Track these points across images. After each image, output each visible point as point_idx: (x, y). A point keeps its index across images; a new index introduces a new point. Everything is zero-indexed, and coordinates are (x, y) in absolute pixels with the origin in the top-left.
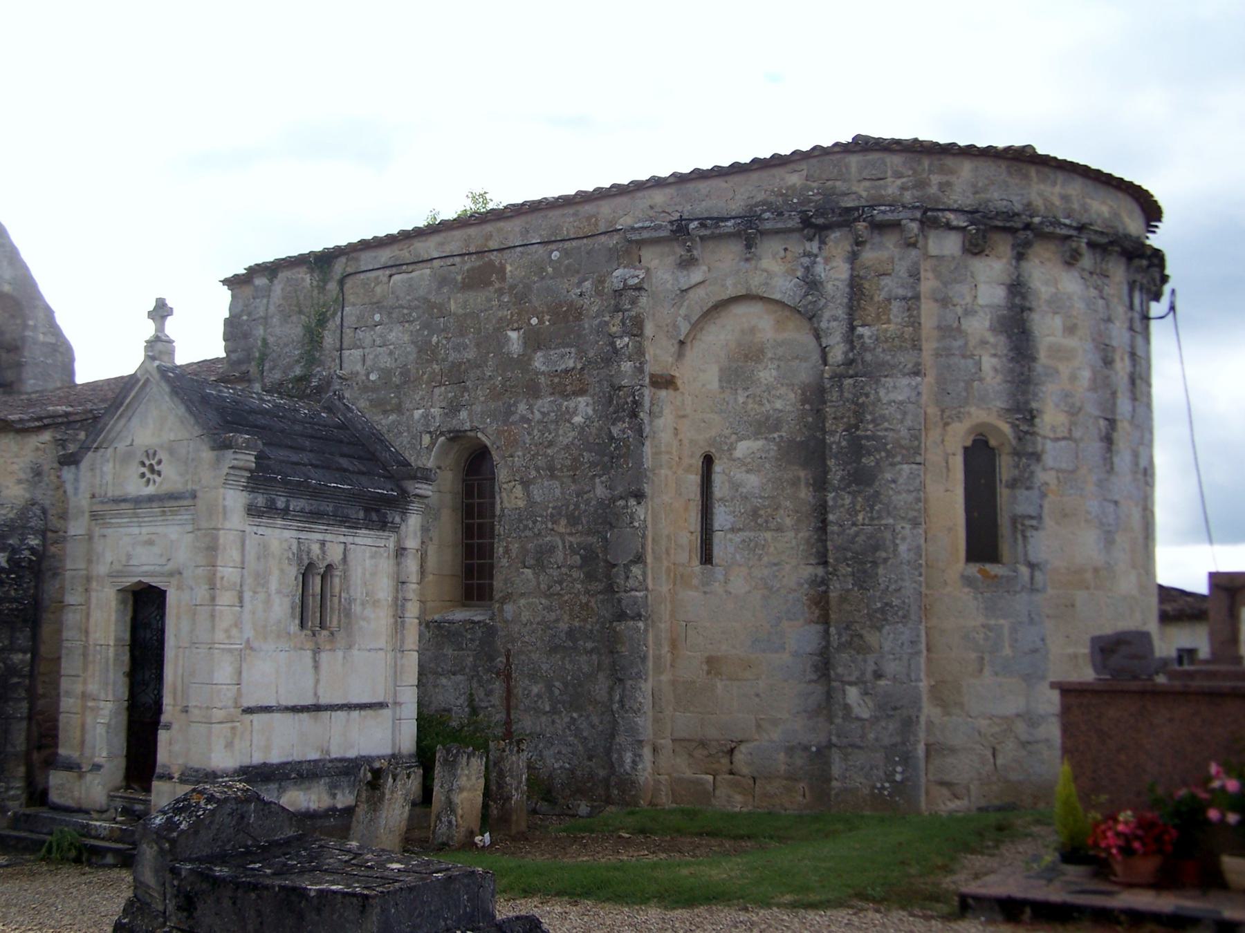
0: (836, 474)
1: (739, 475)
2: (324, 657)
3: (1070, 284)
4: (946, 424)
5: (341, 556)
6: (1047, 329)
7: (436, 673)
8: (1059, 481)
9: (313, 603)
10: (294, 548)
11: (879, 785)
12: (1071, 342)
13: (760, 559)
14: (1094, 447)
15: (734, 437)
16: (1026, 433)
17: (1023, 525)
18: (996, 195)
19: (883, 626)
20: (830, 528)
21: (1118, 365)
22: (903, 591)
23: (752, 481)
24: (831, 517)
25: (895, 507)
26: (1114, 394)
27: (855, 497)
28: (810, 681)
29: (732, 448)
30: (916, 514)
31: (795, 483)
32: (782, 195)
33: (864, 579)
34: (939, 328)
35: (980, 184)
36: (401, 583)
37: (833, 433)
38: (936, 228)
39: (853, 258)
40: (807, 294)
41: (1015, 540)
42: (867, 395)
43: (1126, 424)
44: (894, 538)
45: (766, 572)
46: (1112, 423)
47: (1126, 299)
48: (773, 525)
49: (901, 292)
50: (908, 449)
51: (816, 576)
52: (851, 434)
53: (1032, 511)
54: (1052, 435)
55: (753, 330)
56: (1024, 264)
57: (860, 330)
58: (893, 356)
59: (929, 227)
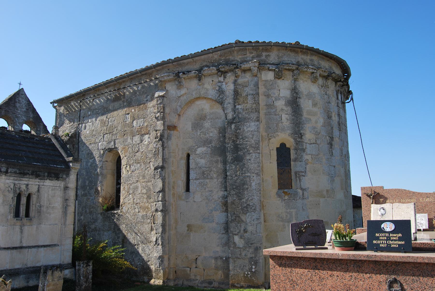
0: (229, 157)
1: (199, 160)
2: (26, 228)
3: (314, 89)
4: (270, 139)
5: (37, 190)
6: (306, 105)
7: (103, 230)
8: (312, 159)
9: (23, 209)
10: (12, 186)
11: (246, 273)
12: (315, 109)
13: (205, 189)
14: (325, 147)
15: (196, 147)
16: (299, 142)
17: (299, 175)
18: (286, 59)
19: (247, 213)
20: (228, 178)
21: (333, 118)
22: (254, 199)
23: (202, 162)
24: (228, 174)
25: (250, 169)
26: (332, 128)
27: (236, 166)
28: (223, 234)
29: (196, 150)
30: (258, 171)
31: (217, 162)
32: (212, 62)
33: (240, 196)
34: (266, 105)
35: (280, 55)
36: (66, 200)
37: (228, 144)
38: (265, 70)
39: (235, 82)
40: (219, 96)
41: (297, 180)
42: (240, 129)
43: (337, 139)
44: (250, 180)
45: (207, 194)
46: (332, 138)
47: (336, 96)
48: (209, 177)
49: (251, 92)
50: (254, 148)
51: (224, 195)
52: (234, 143)
53: (302, 169)
54: (309, 142)
55: (202, 110)
56: (297, 82)
57: (237, 107)
58: (249, 115)
59: (262, 70)
